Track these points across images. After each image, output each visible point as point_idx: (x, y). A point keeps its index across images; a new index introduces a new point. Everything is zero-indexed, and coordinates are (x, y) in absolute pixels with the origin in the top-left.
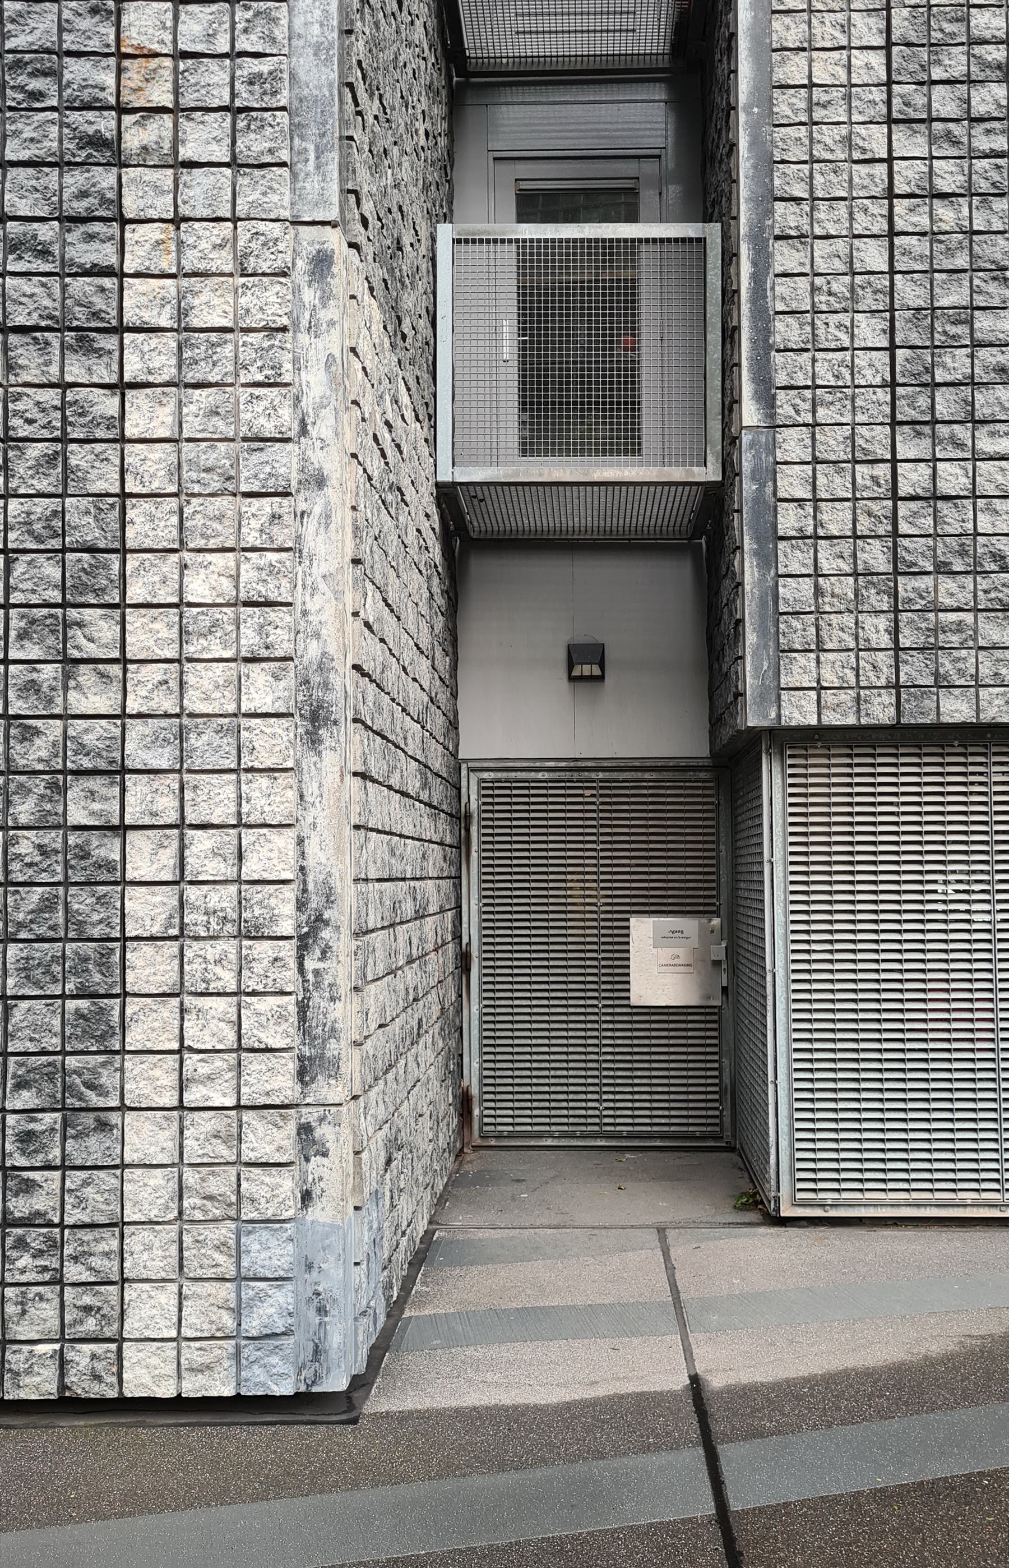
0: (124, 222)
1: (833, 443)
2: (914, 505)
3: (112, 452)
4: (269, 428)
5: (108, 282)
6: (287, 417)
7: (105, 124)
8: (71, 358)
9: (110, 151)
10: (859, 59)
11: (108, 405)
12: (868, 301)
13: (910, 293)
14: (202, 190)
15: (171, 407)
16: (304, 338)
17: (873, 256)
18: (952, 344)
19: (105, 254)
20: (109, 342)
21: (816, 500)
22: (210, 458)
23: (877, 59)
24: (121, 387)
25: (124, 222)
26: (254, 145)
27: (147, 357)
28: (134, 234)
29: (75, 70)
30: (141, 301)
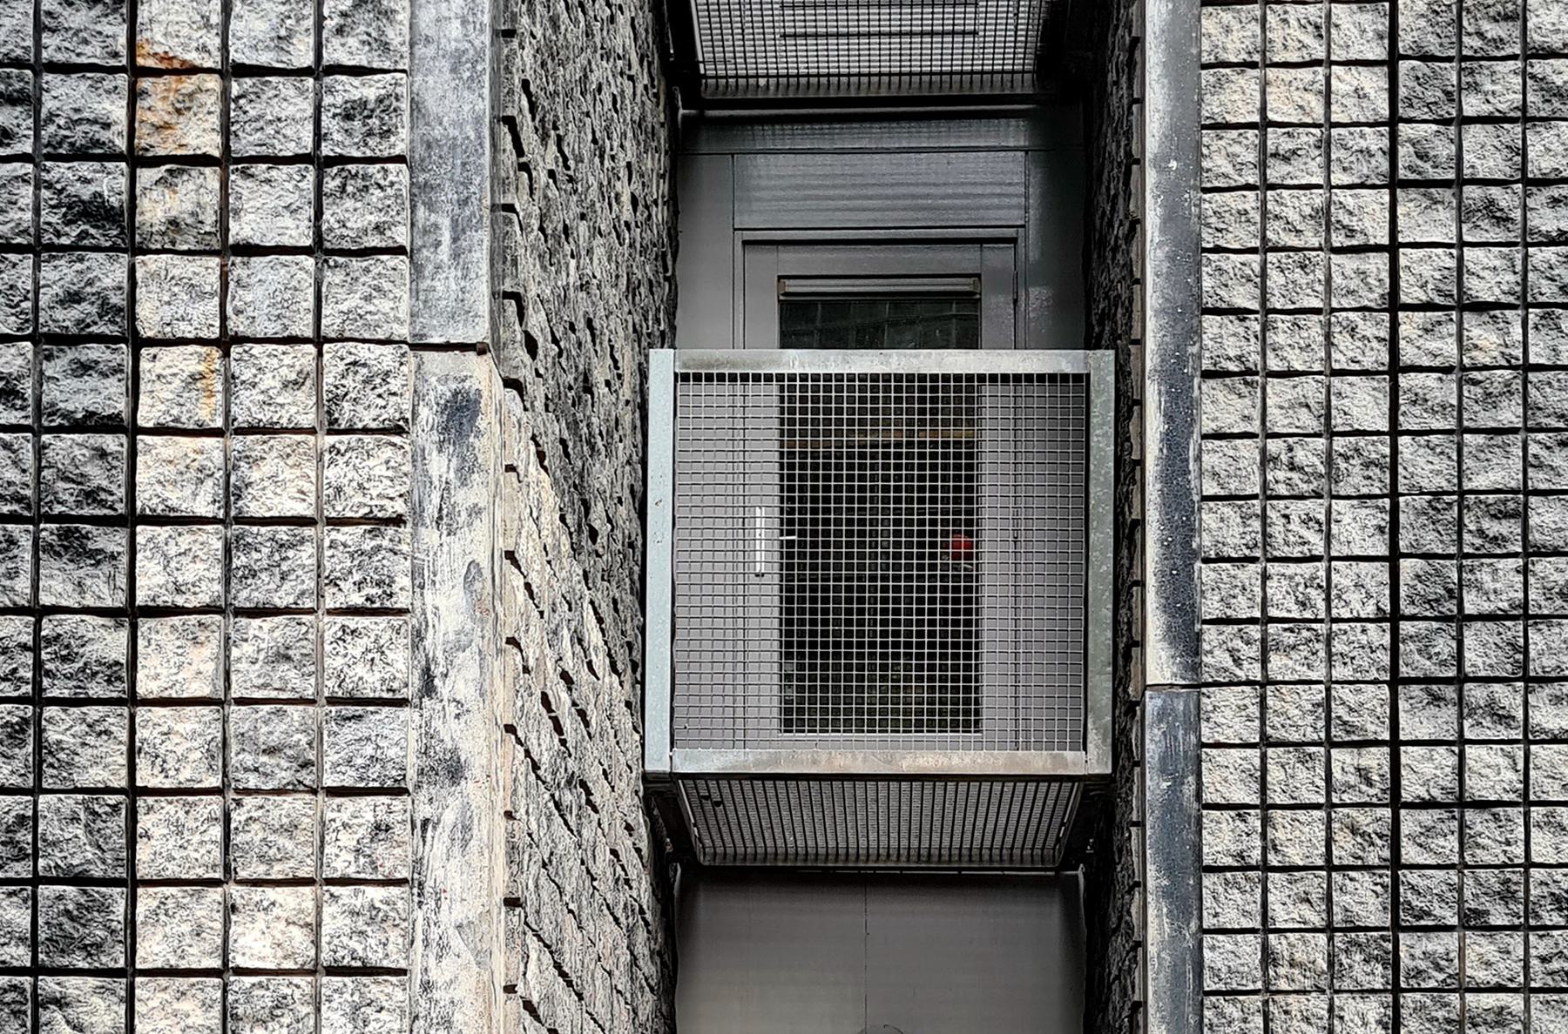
0: (139, 344)
1: (1295, 713)
2: (1427, 817)
3: (115, 720)
4: (371, 682)
5: (111, 442)
6: (400, 666)
7: (109, 183)
8: (49, 565)
9: (115, 225)
10: (1344, 80)
11: (110, 643)
12: (1355, 479)
13: (1424, 466)
14: (267, 291)
15: (212, 647)
16: (430, 536)
17: (1364, 405)
18: (1493, 549)
19: (108, 396)
20: (112, 541)
21: (1265, 807)
22: (275, 731)
23: (1374, 83)
24: (131, 614)
25: (139, 344)
26: (351, 217)
27: (174, 565)
28: (155, 364)
29: (62, 94)
30: (164, 473)
